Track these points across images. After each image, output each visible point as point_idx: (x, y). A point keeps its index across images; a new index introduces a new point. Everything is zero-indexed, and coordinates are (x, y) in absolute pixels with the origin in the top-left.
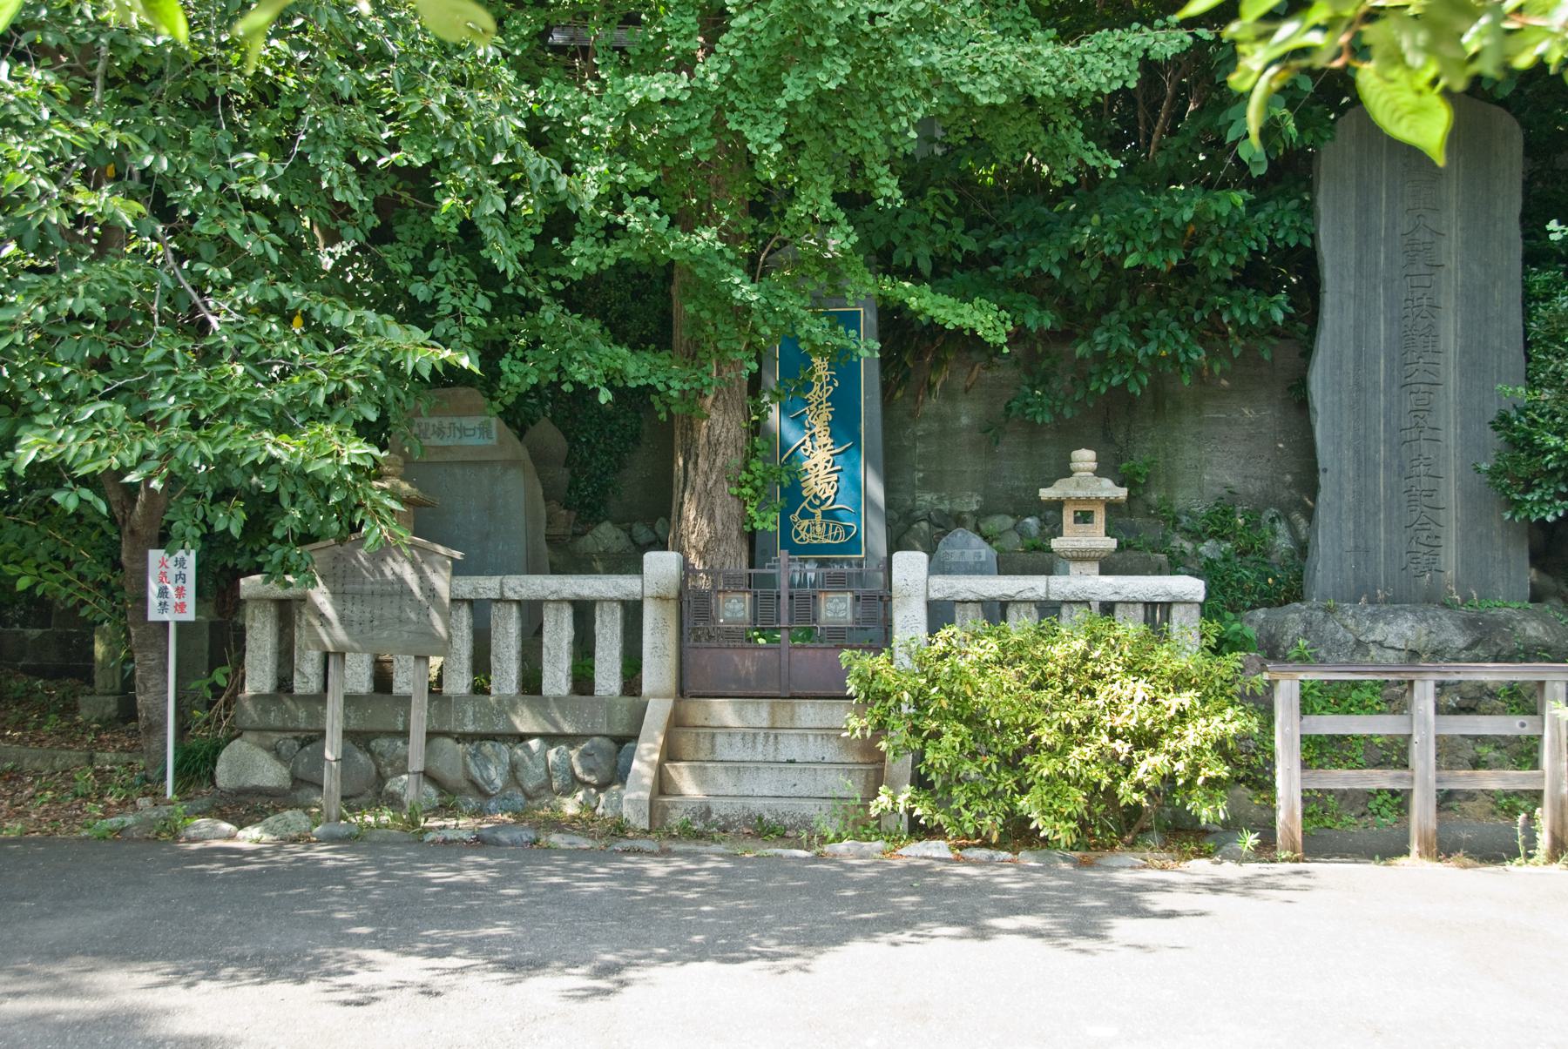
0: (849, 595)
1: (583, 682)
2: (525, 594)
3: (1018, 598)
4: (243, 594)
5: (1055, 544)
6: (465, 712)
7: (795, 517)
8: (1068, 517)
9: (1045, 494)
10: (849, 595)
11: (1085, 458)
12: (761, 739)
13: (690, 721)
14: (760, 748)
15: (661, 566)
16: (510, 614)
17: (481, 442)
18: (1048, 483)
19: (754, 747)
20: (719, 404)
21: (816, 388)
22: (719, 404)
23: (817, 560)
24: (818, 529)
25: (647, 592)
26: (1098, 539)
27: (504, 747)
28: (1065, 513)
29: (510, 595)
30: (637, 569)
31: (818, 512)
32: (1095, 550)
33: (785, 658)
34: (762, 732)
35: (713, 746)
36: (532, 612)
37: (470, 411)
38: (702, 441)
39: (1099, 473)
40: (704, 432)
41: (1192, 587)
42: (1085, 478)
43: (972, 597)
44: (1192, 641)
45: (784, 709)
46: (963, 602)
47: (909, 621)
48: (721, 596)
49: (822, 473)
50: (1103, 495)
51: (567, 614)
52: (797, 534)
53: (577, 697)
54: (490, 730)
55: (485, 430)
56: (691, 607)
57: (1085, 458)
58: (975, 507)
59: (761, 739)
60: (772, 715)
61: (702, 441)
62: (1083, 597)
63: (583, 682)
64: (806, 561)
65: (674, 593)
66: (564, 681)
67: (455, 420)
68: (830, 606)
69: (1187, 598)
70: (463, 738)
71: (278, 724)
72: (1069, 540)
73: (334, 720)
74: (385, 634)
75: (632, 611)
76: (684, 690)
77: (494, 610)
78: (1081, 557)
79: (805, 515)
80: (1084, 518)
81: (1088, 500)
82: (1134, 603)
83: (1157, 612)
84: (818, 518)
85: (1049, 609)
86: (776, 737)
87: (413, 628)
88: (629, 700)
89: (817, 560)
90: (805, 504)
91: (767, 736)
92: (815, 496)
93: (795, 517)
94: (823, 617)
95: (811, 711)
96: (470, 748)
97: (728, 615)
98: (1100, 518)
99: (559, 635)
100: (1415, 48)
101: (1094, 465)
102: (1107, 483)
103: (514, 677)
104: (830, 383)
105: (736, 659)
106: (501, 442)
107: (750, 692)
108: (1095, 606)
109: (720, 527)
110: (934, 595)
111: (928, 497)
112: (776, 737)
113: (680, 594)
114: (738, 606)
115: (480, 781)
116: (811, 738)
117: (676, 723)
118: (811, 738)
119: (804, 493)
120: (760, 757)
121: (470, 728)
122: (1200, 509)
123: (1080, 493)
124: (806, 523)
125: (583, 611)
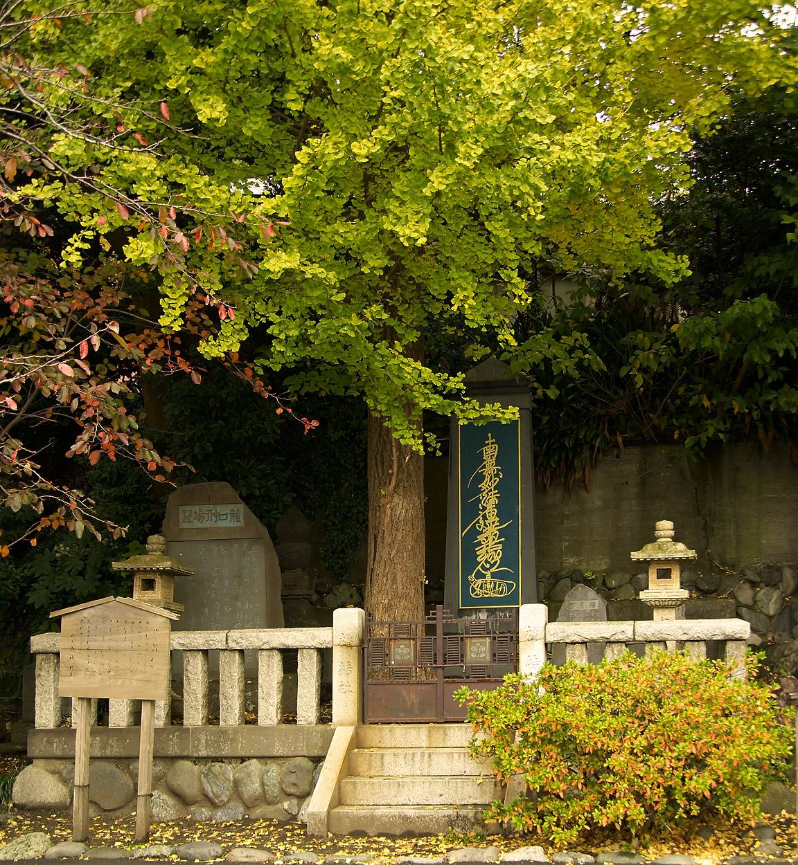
0: (488, 640)
1: (289, 711)
2: (244, 644)
3: (612, 639)
4: (34, 648)
5: (643, 595)
6: (199, 740)
7: (472, 577)
8: (137, 583)
9: (636, 555)
10: (488, 640)
11: (665, 527)
12: (418, 757)
13: (368, 743)
14: (418, 765)
15: (348, 620)
16: (234, 661)
17: (232, 524)
18: (639, 548)
19: (413, 764)
20: (401, 491)
21: (487, 479)
22: (401, 491)
23: (488, 610)
24: (488, 586)
25: (336, 641)
26: (673, 589)
27: (229, 767)
28: (650, 571)
29: (233, 645)
30: (328, 622)
31: (488, 573)
32: (671, 600)
33: (440, 691)
34: (419, 751)
35: (382, 764)
36: (289, 657)
37: (223, 501)
38: (387, 519)
39: (676, 539)
40: (389, 512)
41: (739, 627)
42: (667, 542)
43: (578, 639)
44: (740, 673)
45: (438, 731)
46: (573, 643)
47: (532, 659)
48: (392, 643)
49: (491, 543)
50: (677, 556)
51: (277, 659)
52: (474, 590)
53: (284, 726)
54: (218, 754)
55: (234, 515)
56: (369, 650)
57: (665, 527)
58: (604, 567)
59: (418, 757)
60: (429, 737)
61: (387, 519)
62: (659, 637)
63: (289, 711)
64: (480, 610)
65: (356, 642)
66: (274, 713)
67: (211, 507)
68: (474, 649)
69: (737, 636)
70: (197, 760)
71: (59, 753)
72: (658, 590)
73: (146, 748)
74: (119, 682)
75: (325, 655)
76: (364, 716)
77: (222, 656)
78: (664, 605)
79: (480, 576)
80: (664, 574)
81: (667, 561)
82: (698, 641)
83: (716, 649)
84: (489, 578)
85: (636, 646)
86: (430, 756)
87: (141, 677)
88: (321, 727)
89: (488, 610)
90: (479, 567)
91: (423, 755)
92: (487, 562)
93: (472, 577)
94: (468, 658)
95: (458, 733)
96: (204, 769)
97: (398, 657)
98: (676, 575)
99: (231, 675)
100: (277, 207)
101: (672, 533)
102: (681, 546)
103: (237, 711)
104: (496, 476)
105: (404, 693)
106: (246, 524)
107: (414, 719)
108: (671, 645)
109: (400, 587)
110: (550, 639)
111: (571, 560)
112: (430, 756)
113: (362, 641)
114: (405, 651)
115: (211, 795)
116: (456, 756)
117: (357, 742)
118: (456, 756)
119: (479, 559)
120: (418, 772)
121: (203, 753)
122: (759, 563)
123: (661, 556)
124: (480, 581)
125: (289, 657)
